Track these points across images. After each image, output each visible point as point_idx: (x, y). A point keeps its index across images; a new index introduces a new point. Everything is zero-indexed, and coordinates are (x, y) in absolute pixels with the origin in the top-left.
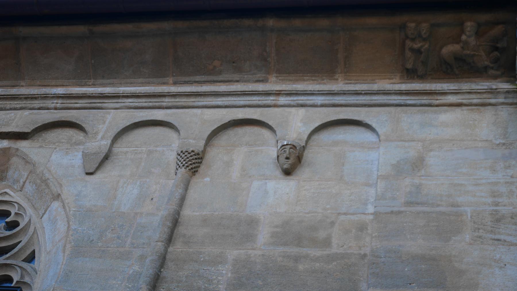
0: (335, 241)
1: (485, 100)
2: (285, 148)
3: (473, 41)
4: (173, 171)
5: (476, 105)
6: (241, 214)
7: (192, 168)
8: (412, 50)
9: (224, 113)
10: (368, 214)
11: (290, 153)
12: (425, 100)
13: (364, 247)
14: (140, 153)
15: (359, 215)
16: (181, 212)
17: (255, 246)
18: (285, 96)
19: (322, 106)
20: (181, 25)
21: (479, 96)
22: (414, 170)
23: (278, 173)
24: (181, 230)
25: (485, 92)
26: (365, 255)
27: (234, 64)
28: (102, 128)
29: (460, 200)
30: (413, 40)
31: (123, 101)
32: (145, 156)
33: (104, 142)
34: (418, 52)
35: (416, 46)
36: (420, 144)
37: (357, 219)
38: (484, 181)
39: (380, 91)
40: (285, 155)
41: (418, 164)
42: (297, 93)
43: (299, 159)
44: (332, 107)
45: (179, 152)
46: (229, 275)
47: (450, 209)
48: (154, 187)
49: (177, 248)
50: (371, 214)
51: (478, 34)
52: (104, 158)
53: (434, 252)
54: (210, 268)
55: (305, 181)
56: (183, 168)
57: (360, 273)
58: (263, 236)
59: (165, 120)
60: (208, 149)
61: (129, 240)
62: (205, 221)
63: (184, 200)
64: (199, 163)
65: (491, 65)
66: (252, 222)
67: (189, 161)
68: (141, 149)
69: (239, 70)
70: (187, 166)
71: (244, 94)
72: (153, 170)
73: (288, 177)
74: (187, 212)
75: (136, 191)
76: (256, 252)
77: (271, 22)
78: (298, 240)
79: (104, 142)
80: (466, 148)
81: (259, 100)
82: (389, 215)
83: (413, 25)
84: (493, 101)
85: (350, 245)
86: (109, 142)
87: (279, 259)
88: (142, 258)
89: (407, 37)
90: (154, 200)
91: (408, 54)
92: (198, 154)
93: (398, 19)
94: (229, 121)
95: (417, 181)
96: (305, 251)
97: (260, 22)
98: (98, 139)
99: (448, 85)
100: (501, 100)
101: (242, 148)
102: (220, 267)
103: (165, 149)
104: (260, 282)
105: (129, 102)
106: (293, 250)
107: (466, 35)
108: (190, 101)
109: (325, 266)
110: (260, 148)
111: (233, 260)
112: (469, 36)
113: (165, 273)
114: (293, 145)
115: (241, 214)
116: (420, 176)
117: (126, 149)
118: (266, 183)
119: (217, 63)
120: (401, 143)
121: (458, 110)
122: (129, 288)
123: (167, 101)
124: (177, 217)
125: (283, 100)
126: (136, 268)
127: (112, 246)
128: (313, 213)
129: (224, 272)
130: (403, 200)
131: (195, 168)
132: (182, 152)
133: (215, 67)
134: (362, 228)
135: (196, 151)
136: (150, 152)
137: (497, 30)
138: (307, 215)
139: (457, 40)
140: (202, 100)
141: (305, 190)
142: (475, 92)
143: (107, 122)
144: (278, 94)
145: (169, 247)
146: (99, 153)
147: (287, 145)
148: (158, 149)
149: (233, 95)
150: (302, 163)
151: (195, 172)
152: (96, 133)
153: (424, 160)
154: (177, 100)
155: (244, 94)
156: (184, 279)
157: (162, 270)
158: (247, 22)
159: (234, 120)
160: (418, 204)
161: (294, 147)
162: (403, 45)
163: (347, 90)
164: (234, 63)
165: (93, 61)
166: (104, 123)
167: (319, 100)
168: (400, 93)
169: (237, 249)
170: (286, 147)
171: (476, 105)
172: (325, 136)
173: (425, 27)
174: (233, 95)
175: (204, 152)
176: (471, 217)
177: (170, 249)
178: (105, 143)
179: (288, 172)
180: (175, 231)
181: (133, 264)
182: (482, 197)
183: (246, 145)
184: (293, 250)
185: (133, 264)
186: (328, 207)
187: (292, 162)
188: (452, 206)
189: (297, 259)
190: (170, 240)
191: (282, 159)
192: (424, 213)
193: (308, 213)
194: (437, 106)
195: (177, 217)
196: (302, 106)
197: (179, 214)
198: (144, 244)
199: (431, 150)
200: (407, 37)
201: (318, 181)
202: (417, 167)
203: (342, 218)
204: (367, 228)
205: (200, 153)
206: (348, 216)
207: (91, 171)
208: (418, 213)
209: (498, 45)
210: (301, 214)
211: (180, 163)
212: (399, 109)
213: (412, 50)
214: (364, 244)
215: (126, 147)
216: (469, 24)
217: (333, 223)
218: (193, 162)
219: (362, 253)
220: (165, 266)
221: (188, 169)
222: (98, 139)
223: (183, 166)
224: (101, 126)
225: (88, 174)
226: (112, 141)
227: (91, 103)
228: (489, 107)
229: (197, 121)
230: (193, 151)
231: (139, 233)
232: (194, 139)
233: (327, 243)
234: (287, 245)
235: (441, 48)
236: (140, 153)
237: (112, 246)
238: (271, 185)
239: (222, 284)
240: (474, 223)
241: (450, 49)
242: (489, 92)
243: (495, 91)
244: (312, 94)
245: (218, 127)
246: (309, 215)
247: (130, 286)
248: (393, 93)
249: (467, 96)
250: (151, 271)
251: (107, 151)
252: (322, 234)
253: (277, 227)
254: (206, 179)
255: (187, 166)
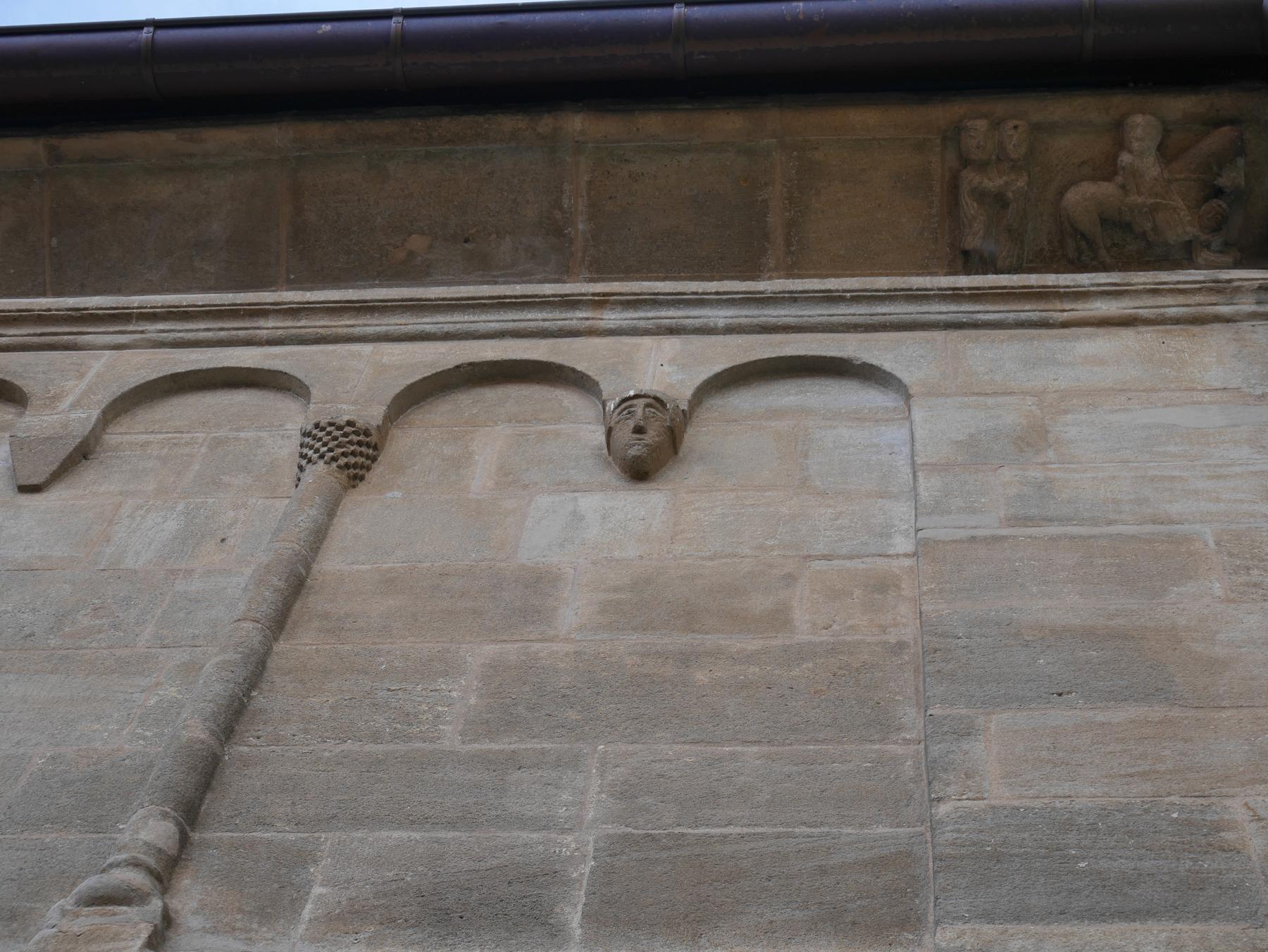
0: (801, 618)
1: (1199, 308)
2: (631, 406)
3: (1151, 168)
4: (289, 480)
5: (1177, 321)
6: (503, 564)
7: (347, 466)
8: (981, 196)
9: (443, 350)
10: (898, 555)
11: (645, 418)
12: (1030, 311)
13: (896, 625)
14: (187, 444)
15: (869, 560)
16: (315, 567)
17: (552, 633)
18: (619, 308)
19: (730, 330)
20: (318, 132)
21: (1181, 299)
22: (1022, 451)
23: (611, 476)
24: (313, 602)
25: (1200, 289)
26: (901, 646)
27: (467, 245)
28: (75, 388)
29: (1175, 509)
30: (982, 166)
31: (140, 329)
32: (203, 450)
33: (80, 414)
34: (1000, 200)
35: (992, 183)
36: (1029, 400)
37: (863, 566)
38: (1238, 469)
39: (896, 290)
40: (631, 424)
41: (1032, 439)
42: (654, 301)
43: (673, 440)
44: (760, 333)
45: (309, 427)
46: (473, 701)
47: (1149, 528)
48: (232, 514)
49: (301, 644)
50: (906, 555)
51: (1165, 153)
52: (76, 449)
53: (1121, 621)
54: (410, 687)
55: (693, 492)
56: (321, 463)
57: (892, 684)
58: (573, 611)
59: (266, 367)
60: (395, 432)
61: (150, 629)
62: (389, 583)
63: (324, 537)
64: (368, 457)
65: (1204, 237)
66: (541, 582)
67: (337, 446)
68: (190, 435)
69: (481, 265)
70: (334, 459)
71: (501, 304)
72: (226, 479)
73: (642, 485)
74: (331, 563)
75: (172, 525)
76: (555, 647)
77: (576, 123)
78: (689, 617)
79: (80, 414)
80: (1166, 406)
81: (544, 320)
82: (966, 545)
83: (982, 124)
84: (1225, 310)
85: (849, 623)
86: (95, 414)
87: (628, 661)
88: (190, 669)
89: (965, 162)
90: (231, 542)
91: (970, 206)
92: (367, 433)
93: (941, 113)
94: (458, 367)
95: (1035, 473)
96: (710, 641)
97: (546, 123)
98: (60, 409)
99: (1090, 275)
100: (1247, 307)
101: (497, 428)
102: (441, 684)
103: (264, 434)
104: (572, 715)
105: (153, 329)
106: (677, 641)
107: (1130, 152)
108: (342, 324)
109: (776, 672)
110: (551, 427)
111: (483, 665)
112: (1142, 156)
113: (259, 700)
114: (656, 398)
115: (503, 564)
116: (1044, 463)
117: (144, 436)
118: (576, 499)
119: (417, 243)
120: (974, 398)
121: (1127, 337)
122: (145, 738)
123: (269, 326)
124: (303, 572)
125: (612, 318)
126: (172, 692)
127: (94, 644)
128: (726, 556)
129: (454, 694)
130: (1002, 514)
131: (355, 466)
132: (317, 426)
133: (411, 254)
134: (882, 586)
135: (360, 423)
136: (218, 443)
137: (1218, 139)
138: (710, 563)
139: (1107, 169)
140: (375, 322)
141: (694, 510)
142: (1171, 291)
143: (91, 374)
144: (601, 302)
145: (276, 639)
146: (61, 438)
147: (636, 397)
148: (242, 435)
149: (469, 306)
150: (681, 454)
151: (355, 477)
152: (56, 398)
153: (1047, 432)
154: (302, 323)
155: (501, 304)
156: (326, 713)
157: (254, 694)
158: (508, 123)
159: (470, 364)
160: (1050, 520)
161: (657, 402)
162: (953, 188)
163: (800, 289)
164: (466, 241)
165: (54, 241)
166: (82, 376)
167: (720, 316)
168: (955, 295)
169: (495, 641)
170: (635, 402)
171: (1177, 321)
172: (745, 400)
173: (1014, 140)
174: (469, 306)
175: (383, 430)
176: (1217, 544)
177: (281, 646)
178: (83, 416)
179: (639, 472)
180: (297, 606)
181: (157, 684)
182: (1242, 501)
183: (510, 421)
184: (677, 641)
185: (157, 684)
186: (770, 543)
187: (650, 448)
188: (1154, 522)
189: (686, 658)
190: (279, 622)
191: (624, 434)
192: (1072, 538)
193: (711, 559)
194: (1065, 325)
195: (303, 572)
196: (672, 331)
197: (308, 568)
198: (195, 637)
199: (1066, 412)
200: (965, 162)
201: (732, 490)
202: (1028, 444)
203: (818, 565)
204: (898, 587)
205: (373, 432)
206: (835, 562)
207: (35, 481)
208: (1054, 539)
209: (1222, 181)
210: (689, 561)
211: (310, 453)
212: (955, 334)
213: (981, 196)
214: (894, 619)
215: (146, 433)
216: (1139, 119)
217: (790, 579)
218: (352, 453)
219: (893, 640)
220: (263, 685)
221: (334, 465)
222: (60, 409)
223: (322, 457)
224: (71, 383)
225: (25, 489)
226: (104, 412)
227: (41, 335)
228: (1217, 326)
229: (357, 373)
230: (350, 423)
231: (182, 615)
232: (355, 403)
233: (779, 619)
234: (654, 628)
235: (1061, 193)
236: (187, 444)
237: (94, 644)
238: (589, 503)
239: (450, 723)
240: (1231, 555)
241: (1084, 197)
242: (1211, 289)
243: (1226, 285)
244: (700, 301)
245: (425, 379)
246: (716, 562)
247: (148, 733)
248: (934, 295)
249: (1150, 301)
250: (218, 688)
251: (86, 433)
252: (760, 603)
253: (616, 589)
254: (389, 495)
255: (334, 459)
